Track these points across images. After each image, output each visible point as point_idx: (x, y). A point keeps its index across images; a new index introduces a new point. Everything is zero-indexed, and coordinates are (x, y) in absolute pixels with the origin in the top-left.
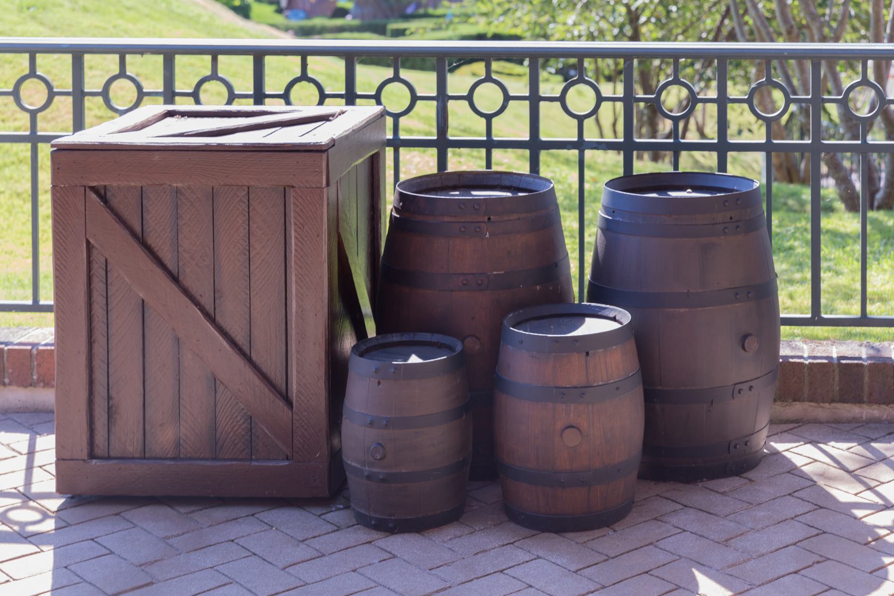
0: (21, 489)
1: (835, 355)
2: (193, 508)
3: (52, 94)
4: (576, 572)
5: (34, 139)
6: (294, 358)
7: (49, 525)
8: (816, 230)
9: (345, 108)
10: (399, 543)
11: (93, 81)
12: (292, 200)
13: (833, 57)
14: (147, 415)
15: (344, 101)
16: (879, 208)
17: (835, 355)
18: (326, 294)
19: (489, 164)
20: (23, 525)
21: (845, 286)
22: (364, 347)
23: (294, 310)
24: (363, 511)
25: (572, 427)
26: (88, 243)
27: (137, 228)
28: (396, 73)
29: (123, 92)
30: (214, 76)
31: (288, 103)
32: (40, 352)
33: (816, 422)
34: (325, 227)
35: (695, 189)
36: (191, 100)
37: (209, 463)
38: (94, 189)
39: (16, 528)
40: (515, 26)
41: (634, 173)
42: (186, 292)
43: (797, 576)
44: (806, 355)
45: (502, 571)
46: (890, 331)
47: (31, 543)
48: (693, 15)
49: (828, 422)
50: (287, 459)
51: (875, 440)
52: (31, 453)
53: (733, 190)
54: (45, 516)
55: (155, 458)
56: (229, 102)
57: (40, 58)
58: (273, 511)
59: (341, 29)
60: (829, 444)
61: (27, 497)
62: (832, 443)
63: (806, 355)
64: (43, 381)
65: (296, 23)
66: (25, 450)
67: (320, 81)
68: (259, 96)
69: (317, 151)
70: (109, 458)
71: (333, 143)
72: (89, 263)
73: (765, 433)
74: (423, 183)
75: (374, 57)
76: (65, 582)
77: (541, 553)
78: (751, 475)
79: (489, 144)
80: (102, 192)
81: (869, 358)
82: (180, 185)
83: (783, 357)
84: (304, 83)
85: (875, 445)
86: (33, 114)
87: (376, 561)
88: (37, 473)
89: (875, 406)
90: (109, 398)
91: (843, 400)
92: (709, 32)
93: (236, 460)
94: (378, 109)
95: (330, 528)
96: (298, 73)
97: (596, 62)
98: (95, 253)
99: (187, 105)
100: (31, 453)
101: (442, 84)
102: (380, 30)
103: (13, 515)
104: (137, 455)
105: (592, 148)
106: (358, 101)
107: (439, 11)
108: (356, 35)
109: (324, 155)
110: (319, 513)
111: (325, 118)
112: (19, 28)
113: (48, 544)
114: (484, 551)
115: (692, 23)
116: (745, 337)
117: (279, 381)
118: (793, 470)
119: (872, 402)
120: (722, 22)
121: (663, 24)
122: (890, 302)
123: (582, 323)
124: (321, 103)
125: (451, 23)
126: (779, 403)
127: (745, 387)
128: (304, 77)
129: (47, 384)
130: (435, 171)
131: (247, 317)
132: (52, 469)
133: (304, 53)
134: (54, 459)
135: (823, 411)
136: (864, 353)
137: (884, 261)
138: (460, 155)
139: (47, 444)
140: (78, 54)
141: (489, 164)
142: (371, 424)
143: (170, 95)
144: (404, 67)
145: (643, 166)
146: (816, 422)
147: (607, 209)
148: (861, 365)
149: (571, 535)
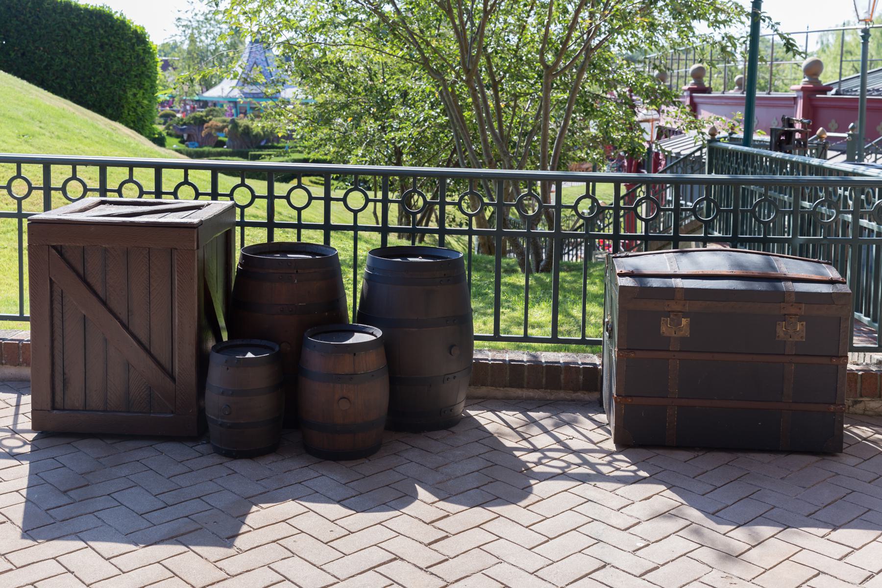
0: (11, 427)
1: (507, 359)
2: (114, 441)
3: (31, 189)
4: (344, 484)
5: (20, 215)
6: (177, 353)
7: (27, 449)
8: (498, 284)
9: (211, 202)
10: (240, 465)
11: (57, 180)
12: (176, 257)
13: (516, 178)
14: (87, 385)
15: (154, 196)
16: (542, 271)
17: (507, 359)
18: (196, 314)
19: (299, 238)
20: (11, 448)
21: (517, 318)
22: (220, 347)
23: (177, 324)
24: (218, 445)
25: (345, 398)
26: (51, 280)
27: (81, 271)
28: (243, 181)
29: (74, 189)
30: (131, 180)
31: (176, 198)
32: (24, 345)
33: (495, 398)
34: (196, 274)
35: (424, 257)
36: (116, 194)
37: (125, 414)
38: (54, 247)
39: (7, 450)
40: (326, 154)
41: (388, 245)
42: (111, 311)
43: (478, 490)
44: (490, 359)
45: (300, 483)
47: (16, 459)
48: (434, 150)
49: (502, 399)
50: (172, 413)
51: (530, 411)
52: (18, 405)
53: (447, 258)
54: (25, 444)
55: (92, 411)
56: (140, 197)
57: (24, 166)
58: (163, 444)
59: (220, 154)
61: (14, 432)
62: (504, 412)
63: (490, 359)
64: (26, 363)
65: (191, 149)
66: (14, 404)
67: (197, 186)
68: (158, 193)
69: (191, 228)
70: (64, 410)
71: (201, 223)
72: (52, 292)
73: (463, 404)
74: (257, 249)
75: (230, 171)
76: (35, 483)
77: (324, 473)
78: (454, 429)
79: (299, 226)
80: (59, 249)
81: (528, 361)
82: (107, 246)
83: (475, 359)
84: (19, 180)
85: (530, 414)
86: (19, 200)
87: (224, 475)
88: (21, 418)
89: (531, 390)
90: (64, 374)
91: (511, 386)
92: (444, 161)
93: (141, 413)
94: (231, 203)
95: (198, 454)
96: (127, 177)
97: (375, 178)
98: (55, 286)
99: (114, 197)
100: (18, 405)
101: (271, 188)
102: (245, 156)
103: (5, 442)
104: (81, 409)
105: (362, 230)
106: (219, 198)
107: (280, 145)
108: (229, 158)
109: (196, 230)
110: (191, 445)
111: (198, 208)
112: (17, 148)
113: (26, 460)
114: (290, 471)
115: (434, 156)
116: (452, 346)
117: (168, 366)
118: (480, 427)
119: (529, 387)
120: (452, 155)
121: (416, 153)
123: (353, 335)
124: (196, 198)
125: (287, 152)
126: (472, 387)
127: (451, 376)
128: (186, 182)
129: (28, 365)
130: (266, 241)
131: (148, 327)
132: (30, 415)
133: (186, 167)
134: (30, 410)
135: (500, 392)
136: (525, 358)
138: (288, 233)
139: (27, 399)
140: (47, 164)
141: (299, 238)
142: (223, 393)
143: (103, 191)
144: (249, 178)
145: (393, 240)
146: (495, 398)
147: (369, 268)
149: (343, 462)
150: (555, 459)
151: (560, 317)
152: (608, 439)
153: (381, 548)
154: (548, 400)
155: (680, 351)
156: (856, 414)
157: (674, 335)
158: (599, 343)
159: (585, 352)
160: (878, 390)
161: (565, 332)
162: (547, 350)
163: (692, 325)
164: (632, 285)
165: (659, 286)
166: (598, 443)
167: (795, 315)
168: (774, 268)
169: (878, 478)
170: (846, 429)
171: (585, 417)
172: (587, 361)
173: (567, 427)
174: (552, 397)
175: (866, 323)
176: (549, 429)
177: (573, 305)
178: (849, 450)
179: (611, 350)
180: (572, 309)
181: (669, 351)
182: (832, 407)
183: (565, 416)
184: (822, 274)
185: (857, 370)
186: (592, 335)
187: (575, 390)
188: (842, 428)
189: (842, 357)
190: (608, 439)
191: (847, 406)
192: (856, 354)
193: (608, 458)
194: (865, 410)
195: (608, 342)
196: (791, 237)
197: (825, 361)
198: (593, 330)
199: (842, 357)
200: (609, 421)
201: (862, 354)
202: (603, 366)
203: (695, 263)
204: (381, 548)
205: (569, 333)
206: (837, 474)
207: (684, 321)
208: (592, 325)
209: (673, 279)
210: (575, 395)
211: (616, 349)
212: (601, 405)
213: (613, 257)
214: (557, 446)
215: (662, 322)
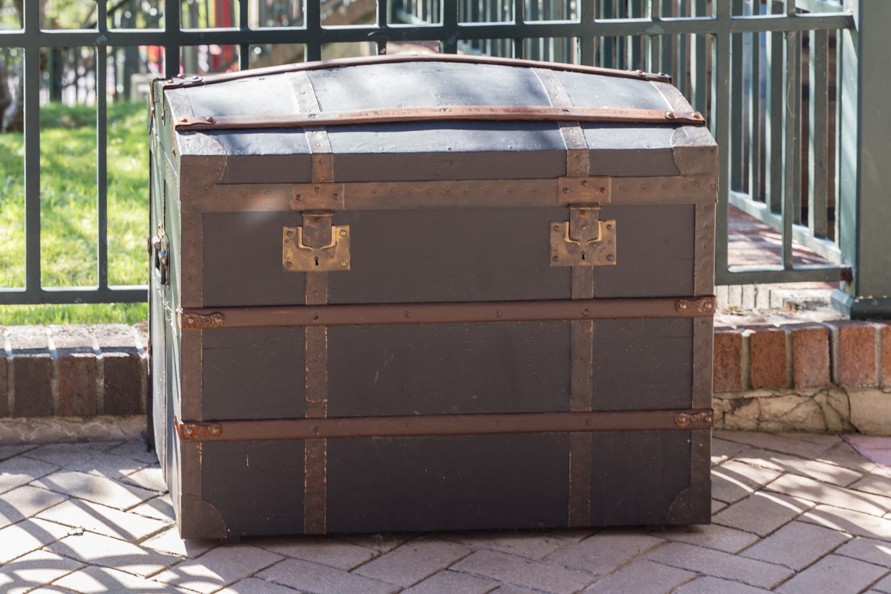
46: (9, 310)
60: (90, 472)
122: (12, 268)
137: (8, 207)
148: (49, 360)
150: (42, 586)
151: (47, 240)
152: (167, 528)
153: (721, 501)
154: (22, 443)
155: (329, 305)
156: (740, 429)
157: (314, 267)
158: (140, 296)
159: (109, 319)
160: (788, 369)
161: (63, 276)
162: (17, 320)
163: (355, 242)
164: (211, 153)
165: (274, 152)
166: (144, 539)
167: (593, 205)
168: (536, 94)
169: (791, 577)
170: (718, 467)
171: (113, 479)
172: (113, 342)
173: (721, 363)
174: (33, 436)
175: (758, 216)
176: (27, 512)
177: (82, 209)
178: (726, 517)
179: (168, 312)
180: (81, 217)
181: (303, 305)
182: (684, 418)
183: (61, 480)
184: (649, 106)
185: (739, 327)
186: (126, 278)
187: (88, 416)
188: (708, 465)
189: (700, 297)
190: (167, 528)
191: (717, 412)
192: (737, 289)
193: (169, 576)
194: (759, 420)
195: (161, 294)
196: (441, 24)
197: (665, 309)
198: (130, 267)
199: (700, 297)
200: (170, 485)
201: (749, 289)
202: (151, 353)
203: (359, 92)
204: (721, 501)
205: (73, 275)
206: (700, 575)
207: (337, 234)
208: (128, 253)
209: (307, 134)
210: (86, 428)
211: (180, 310)
212: (150, 446)
213: (166, 88)
214: (46, 555)
215: (285, 237)
